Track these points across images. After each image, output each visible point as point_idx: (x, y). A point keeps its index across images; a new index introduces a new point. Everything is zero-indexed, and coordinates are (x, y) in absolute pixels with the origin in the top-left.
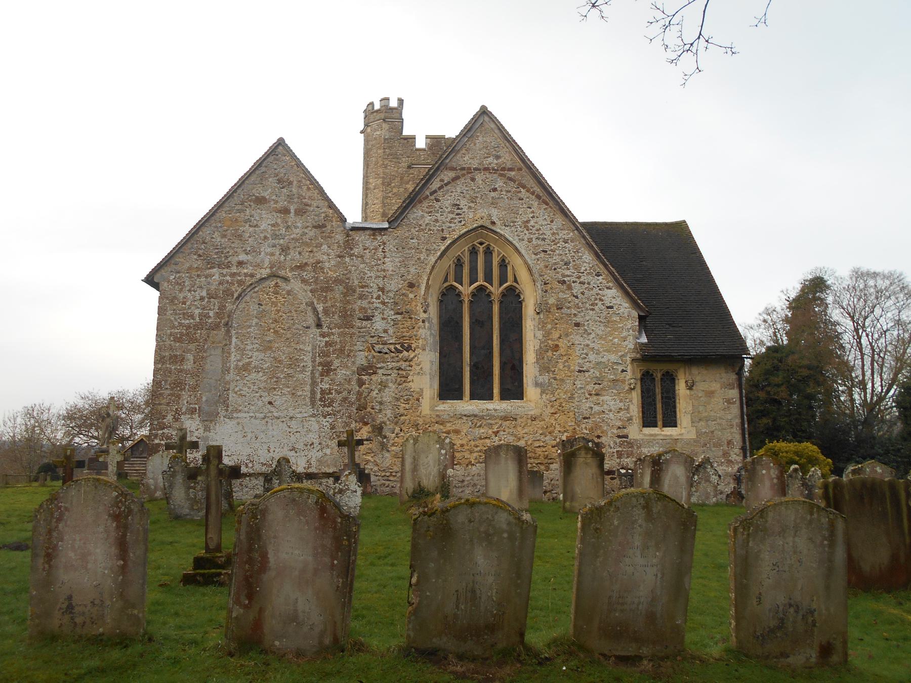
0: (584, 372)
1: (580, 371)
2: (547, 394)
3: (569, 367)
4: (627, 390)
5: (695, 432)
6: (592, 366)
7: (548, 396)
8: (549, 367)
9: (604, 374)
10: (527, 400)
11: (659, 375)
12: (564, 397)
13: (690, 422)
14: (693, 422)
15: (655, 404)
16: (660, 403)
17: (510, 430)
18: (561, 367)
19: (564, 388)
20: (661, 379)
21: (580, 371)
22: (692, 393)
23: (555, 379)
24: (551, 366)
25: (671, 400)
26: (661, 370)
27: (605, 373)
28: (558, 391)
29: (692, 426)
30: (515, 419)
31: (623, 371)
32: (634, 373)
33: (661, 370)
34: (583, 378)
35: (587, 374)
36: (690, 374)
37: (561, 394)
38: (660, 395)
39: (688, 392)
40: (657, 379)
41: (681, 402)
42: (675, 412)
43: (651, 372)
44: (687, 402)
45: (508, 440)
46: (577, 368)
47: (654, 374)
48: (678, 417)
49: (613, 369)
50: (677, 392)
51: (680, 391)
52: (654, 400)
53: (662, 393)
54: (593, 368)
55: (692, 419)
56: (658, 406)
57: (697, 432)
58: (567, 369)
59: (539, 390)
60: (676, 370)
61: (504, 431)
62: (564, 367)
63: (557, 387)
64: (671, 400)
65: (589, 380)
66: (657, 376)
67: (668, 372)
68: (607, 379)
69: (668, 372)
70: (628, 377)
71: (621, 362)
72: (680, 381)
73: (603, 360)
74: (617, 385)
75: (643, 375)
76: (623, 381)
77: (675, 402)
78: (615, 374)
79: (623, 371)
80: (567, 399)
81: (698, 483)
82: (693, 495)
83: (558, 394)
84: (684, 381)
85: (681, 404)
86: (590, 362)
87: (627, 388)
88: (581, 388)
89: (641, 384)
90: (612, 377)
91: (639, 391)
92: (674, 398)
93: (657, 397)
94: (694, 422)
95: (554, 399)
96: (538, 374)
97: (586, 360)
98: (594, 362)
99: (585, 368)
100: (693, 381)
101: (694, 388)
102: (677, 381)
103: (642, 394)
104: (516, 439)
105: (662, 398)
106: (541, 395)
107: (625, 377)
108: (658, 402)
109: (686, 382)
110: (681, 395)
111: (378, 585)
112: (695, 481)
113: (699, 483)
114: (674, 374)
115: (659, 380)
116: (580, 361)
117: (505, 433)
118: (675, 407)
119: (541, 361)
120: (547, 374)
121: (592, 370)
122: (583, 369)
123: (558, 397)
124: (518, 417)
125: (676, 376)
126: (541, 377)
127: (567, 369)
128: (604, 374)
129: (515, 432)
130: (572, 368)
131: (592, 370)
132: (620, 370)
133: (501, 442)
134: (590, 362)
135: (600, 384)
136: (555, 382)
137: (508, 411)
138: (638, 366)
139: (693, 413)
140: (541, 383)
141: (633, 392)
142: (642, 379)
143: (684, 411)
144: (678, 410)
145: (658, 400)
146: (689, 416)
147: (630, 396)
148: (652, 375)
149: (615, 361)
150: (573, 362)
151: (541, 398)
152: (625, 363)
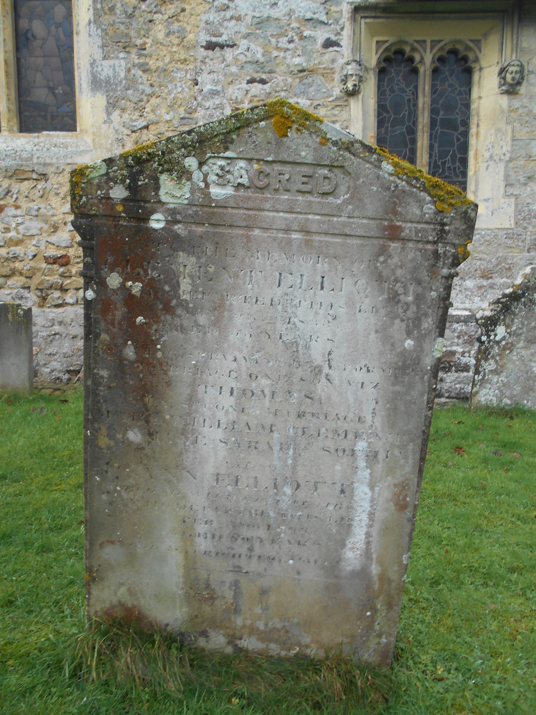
0: (222, 47)
1: (210, 46)
2: (123, 110)
3: (182, 35)
4: (337, 99)
5: (511, 210)
6: (244, 30)
7: (126, 116)
8: (127, 35)
9: (275, 53)
10: (81, 131)
11: (428, 58)
12: (168, 117)
13: (502, 185)
14: (508, 185)
15: (414, 141)
16: (426, 136)
17: (31, 205)
18: (161, 36)
19: (170, 93)
20: (435, 71)
21: (210, 46)
22: (516, 103)
23: (146, 70)
24: (132, 33)
25: (457, 130)
26: (434, 43)
27: (277, 48)
28: (154, 101)
29: (507, 195)
30: (44, 176)
31: (329, 44)
32: (356, 48)
33: (434, 43)
34: (218, 66)
35: (229, 53)
36: (516, 47)
37: (162, 111)
38: (427, 114)
39: (504, 100)
40: (421, 70)
41: (482, 130)
42: (464, 162)
43: (407, 49)
44: (498, 130)
45: (28, 229)
46: (204, 38)
47: (417, 57)
48: (471, 173)
49: (302, 38)
50: (473, 106)
51: (482, 101)
52: (412, 132)
53: (434, 111)
54: (247, 36)
55: (507, 176)
56: (419, 144)
57: (518, 212)
58: (176, 41)
59: (101, 100)
60: (477, 42)
61: (17, 207)
62: (168, 35)
63: (148, 90)
64: (457, 130)
65: (234, 69)
66: (422, 61)
67: (453, 52)
68: (283, 68)
69: (453, 52)
70: (341, 61)
71: (324, 18)
72: (485, 72)
73: (275, 13)
74: (310, 85)
75: (387, 60)
76: (328, 73)
77: (466, 134)
78: (305, 52)
79: (329, 44)
80: (176, 122)
81: (505, 348)
82: (489, 381)
83: (153, 111)
84: (497, 69)
85: (482, 138)
86: (238, 19)
87: (337, 91)
88: (214, 93)
89: (379, 87)
90: (297, 60)
91: (372, 103)
92: (466, 124)
93: (420, 119)
94: (511, 185)
95: (142, 123)
96: (98, 55)
97: (228, 14)
98: (249, 19)
99: (224, 37)
100: (522, 66)
101: (523, 89)
102: (476, 77)
103: (379, 114)
104: (46, 227)
105: (433, 123)
106: (109, 114)
107: (333, 61)
108: (419, 134)
109: (502, 71)
110: (482, 113)
111: (433, 680)
112: (498, 343)
113: (510, 347)
114: (471, 56)
115: (429, 73)
116: (212, 16)
117: (19, 212)
118: (464, 148)
119: (106, 19)
120: (122, 55)
121: (244, 44)
122: (220, 40)
123: (152, 117)
124: (50, 170)
125: (477, 60)
126: (106, 63)
127: (176, 41)
128: (275, 53)
129: (43, 211)
130: (191, 37)
131: (244, 44)
132: (320, 41)
133: (9, 235)
134: (238, 19)
135: (263, 82)
136: (145, 76)
137: (25, 155)
138: (372, 31)
139: (511, 160)
140: (108, 81)
141: (353, 102)
142: (382, 72)
143: (487, 155)
144: (471, 154)
145: (420, 127)
146: (501, 167)
147: (344, 115)
148: (411, 60)
149: (309, 15)
150: (193, 20)
151: (107, 122)
152: (337, 21)
